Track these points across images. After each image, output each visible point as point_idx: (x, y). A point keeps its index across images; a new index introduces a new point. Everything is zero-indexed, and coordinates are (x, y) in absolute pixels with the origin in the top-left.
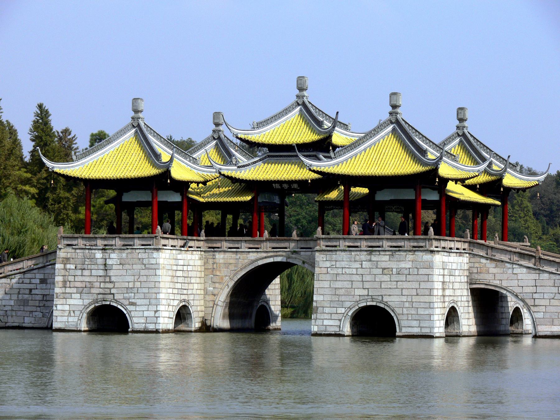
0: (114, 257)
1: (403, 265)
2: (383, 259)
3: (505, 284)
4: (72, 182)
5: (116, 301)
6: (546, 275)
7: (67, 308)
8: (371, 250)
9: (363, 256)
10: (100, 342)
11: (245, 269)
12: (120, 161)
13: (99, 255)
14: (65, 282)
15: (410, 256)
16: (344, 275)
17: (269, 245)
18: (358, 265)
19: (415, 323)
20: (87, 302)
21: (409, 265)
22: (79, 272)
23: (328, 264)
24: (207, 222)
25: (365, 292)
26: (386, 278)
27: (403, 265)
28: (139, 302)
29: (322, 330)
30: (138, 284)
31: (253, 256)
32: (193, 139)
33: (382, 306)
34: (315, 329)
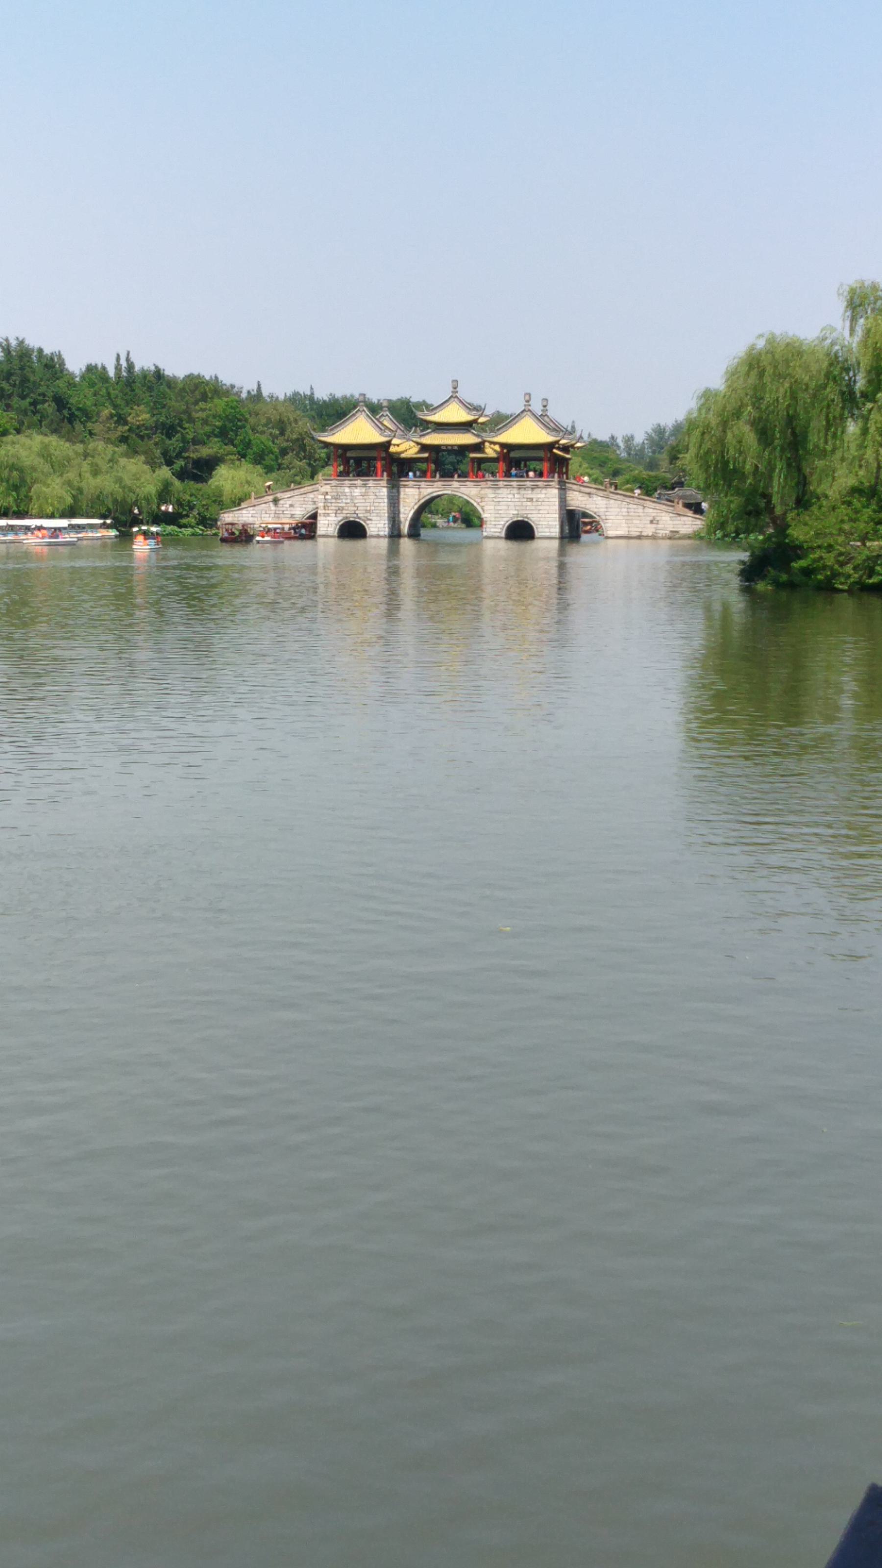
0: (357, 492)
1: (539, 496)
2: (529, 493)
3: (588, 506)
4: (327, 445)
5: (359, 518)
6: (613, 501)
7: (327, 522)
8: (520, 488)
9: (515, 491)
10: (350, 545)
11: (45, 525)
12: (526, 433)
13: (347, 490)
14: (324, 507)
15: (544, 491)
16: (498, 503)
17: (440, 483)
18: (511, 496)
19: (547, 530)
20: (340, 519)
21: (543, 496)
22: (333, 501)
23: (493, 495)
24: (857, 451)
25: (516, 512)
26: (529, 504)
27: (539, 496)
28: (374, 518)
29: (490, 534)
30: (373, 508)
31: (430, 490)
32: (662, 424)
33: (520, 519)
34: (485, 534)
